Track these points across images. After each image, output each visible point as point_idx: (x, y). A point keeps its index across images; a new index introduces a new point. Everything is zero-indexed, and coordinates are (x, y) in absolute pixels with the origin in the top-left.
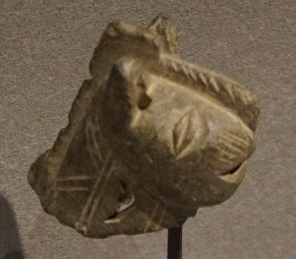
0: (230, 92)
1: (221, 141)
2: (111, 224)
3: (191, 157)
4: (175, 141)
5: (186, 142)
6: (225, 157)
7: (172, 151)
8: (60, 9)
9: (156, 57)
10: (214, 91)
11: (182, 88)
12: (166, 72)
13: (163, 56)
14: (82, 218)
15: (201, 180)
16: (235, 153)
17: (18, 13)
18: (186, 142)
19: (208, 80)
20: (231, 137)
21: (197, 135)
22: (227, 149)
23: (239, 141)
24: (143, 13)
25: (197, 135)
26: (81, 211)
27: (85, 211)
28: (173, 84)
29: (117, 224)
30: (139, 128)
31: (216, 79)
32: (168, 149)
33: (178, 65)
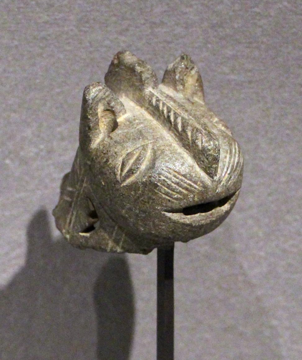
0: (189, 134)
1: (163, 178)
2: (84, 236)
3: (134, 187)
4: (122, 170)
5: (131, 172)
6: (167, 194)
7: (118, 177)
8: (169, 43)
9: (141, 90)
10: (177, 131)
11: (155, 122)
12: (147, 105)
13: (149, 90)
14: (67, 226)
15: (145, 212)
16: (180, 193)
17: (123, 38)
18: (131, 172)
19: (176, 118)
20: (175, 176)
21: (143, 167)
22: (169, 186)
23: (185, 183)
24: (262, 62)
25: (143, 167)
26: (66, 219)
27: (68, 221)
28: (149, 117)
29: (87, 237)
30: (97, 150)
31: (183, 118)
32: (115, 174)
33: (158, 100)
